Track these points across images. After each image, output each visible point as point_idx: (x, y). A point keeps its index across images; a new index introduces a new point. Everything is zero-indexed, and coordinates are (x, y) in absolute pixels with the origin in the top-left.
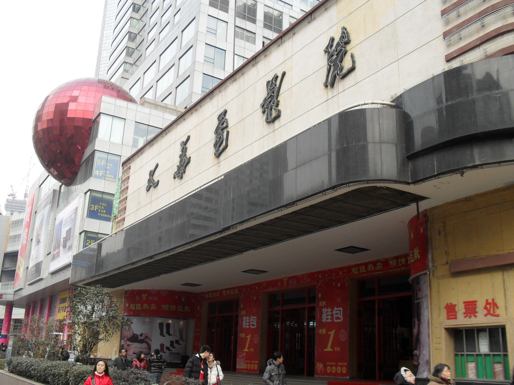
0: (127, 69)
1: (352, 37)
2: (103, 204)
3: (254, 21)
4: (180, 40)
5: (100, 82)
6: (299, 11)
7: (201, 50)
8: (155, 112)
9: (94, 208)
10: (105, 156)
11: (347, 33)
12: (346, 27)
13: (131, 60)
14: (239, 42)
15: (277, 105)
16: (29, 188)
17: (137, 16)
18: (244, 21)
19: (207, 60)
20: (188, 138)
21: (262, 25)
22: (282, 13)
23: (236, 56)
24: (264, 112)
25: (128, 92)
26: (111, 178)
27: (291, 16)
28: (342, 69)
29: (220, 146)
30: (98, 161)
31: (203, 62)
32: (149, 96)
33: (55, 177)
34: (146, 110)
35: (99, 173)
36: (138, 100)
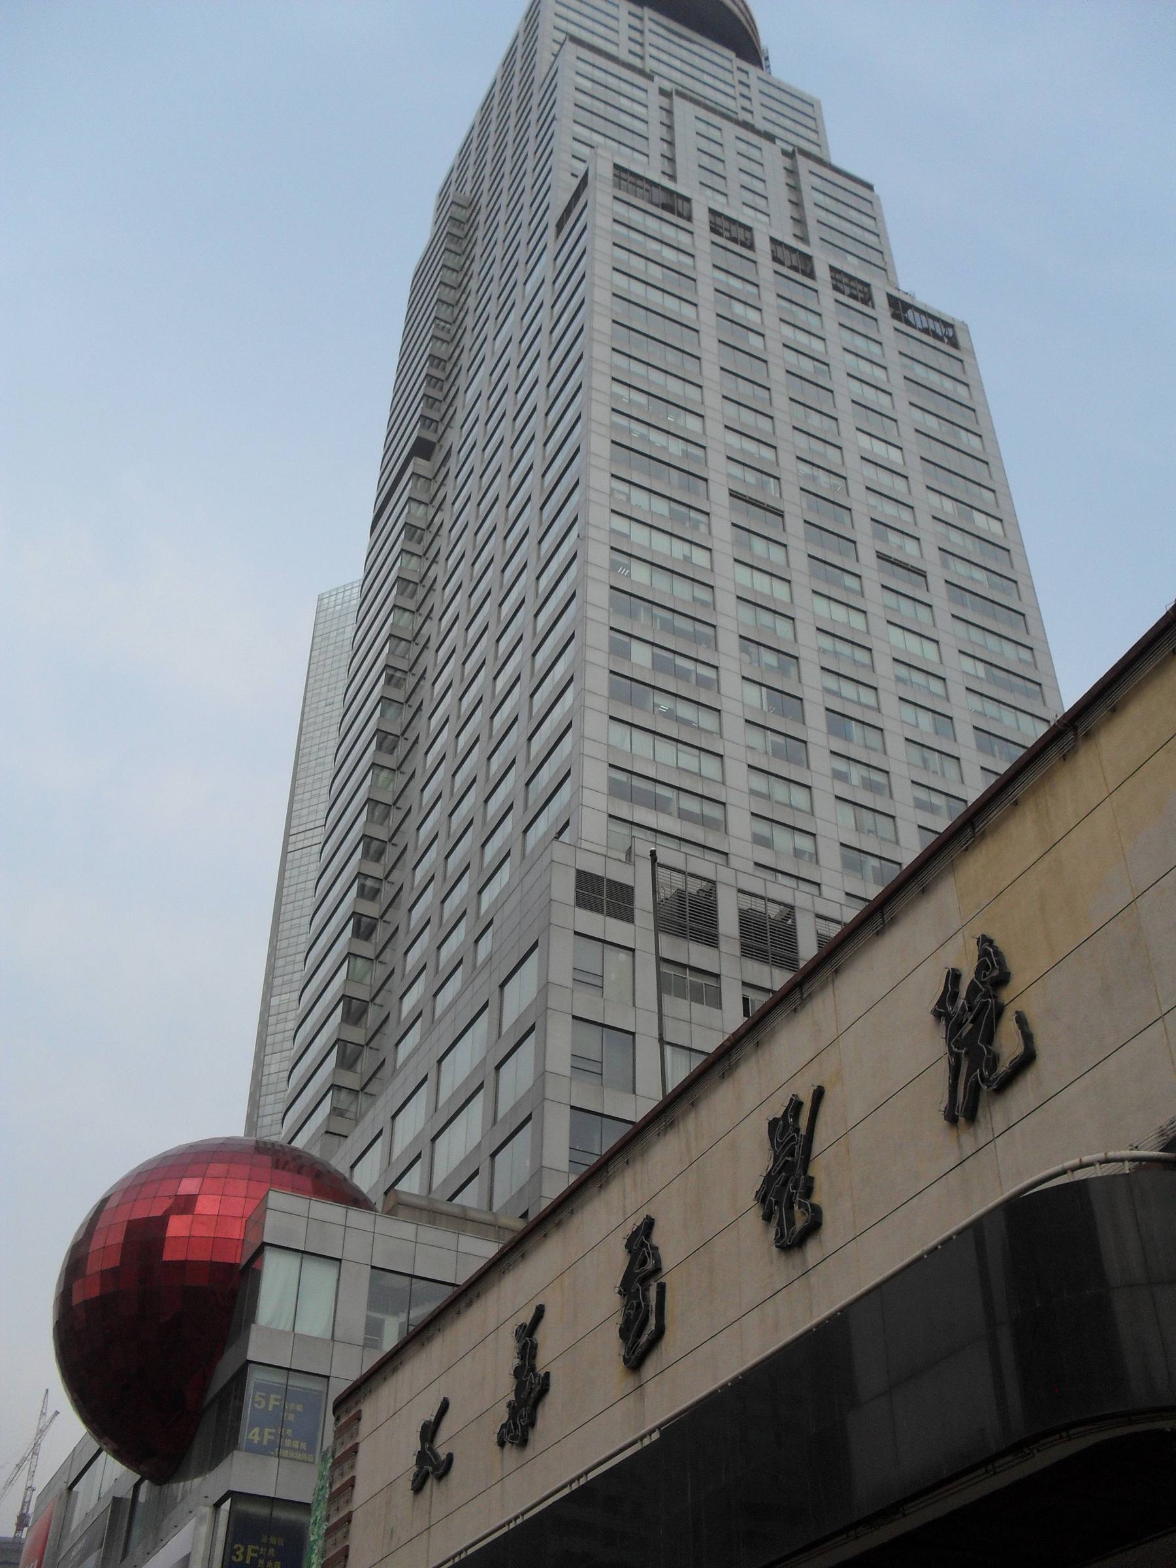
0: (343, 1106)
1: (1014, 963)
2: (273, 1540)
3: (711, 939)
4: (497, 1012)
5: (262, 1148)
6: (842, 898)
7: (561, 1040)
8: (429, 1234)
9: (245, 1554)
10: (278, 1379)
11: (997, 953)
12: (991, 934)
13: (351, 1080)
14: (676, 1006)
15: (809, 1191)
16: (36, 1494)
17: (367, 949)
18: (682, 944)
19: (582, 1066)
20: (540, 1312)
21: (737, 951)
22: (792, 907)
23: (668, 1049)
24: (767, 1217)
25: (347, 1175)
26: (300, 1450)
27: (818, 916)
28: (994, 1060)
29: (641, 1333)
30: (257, 1397)
31: (569, 1074)
32: (411, 1185)
33: (118, 1455)
34: (405, 1229)
35: (261, 1434)
36: (377, 1198)
